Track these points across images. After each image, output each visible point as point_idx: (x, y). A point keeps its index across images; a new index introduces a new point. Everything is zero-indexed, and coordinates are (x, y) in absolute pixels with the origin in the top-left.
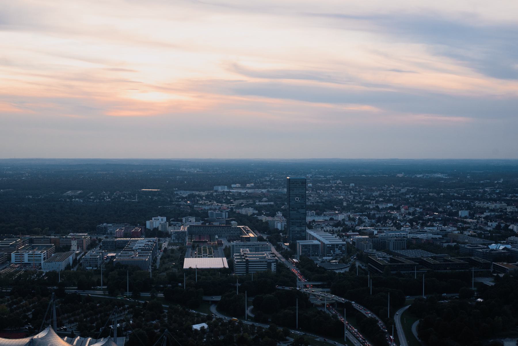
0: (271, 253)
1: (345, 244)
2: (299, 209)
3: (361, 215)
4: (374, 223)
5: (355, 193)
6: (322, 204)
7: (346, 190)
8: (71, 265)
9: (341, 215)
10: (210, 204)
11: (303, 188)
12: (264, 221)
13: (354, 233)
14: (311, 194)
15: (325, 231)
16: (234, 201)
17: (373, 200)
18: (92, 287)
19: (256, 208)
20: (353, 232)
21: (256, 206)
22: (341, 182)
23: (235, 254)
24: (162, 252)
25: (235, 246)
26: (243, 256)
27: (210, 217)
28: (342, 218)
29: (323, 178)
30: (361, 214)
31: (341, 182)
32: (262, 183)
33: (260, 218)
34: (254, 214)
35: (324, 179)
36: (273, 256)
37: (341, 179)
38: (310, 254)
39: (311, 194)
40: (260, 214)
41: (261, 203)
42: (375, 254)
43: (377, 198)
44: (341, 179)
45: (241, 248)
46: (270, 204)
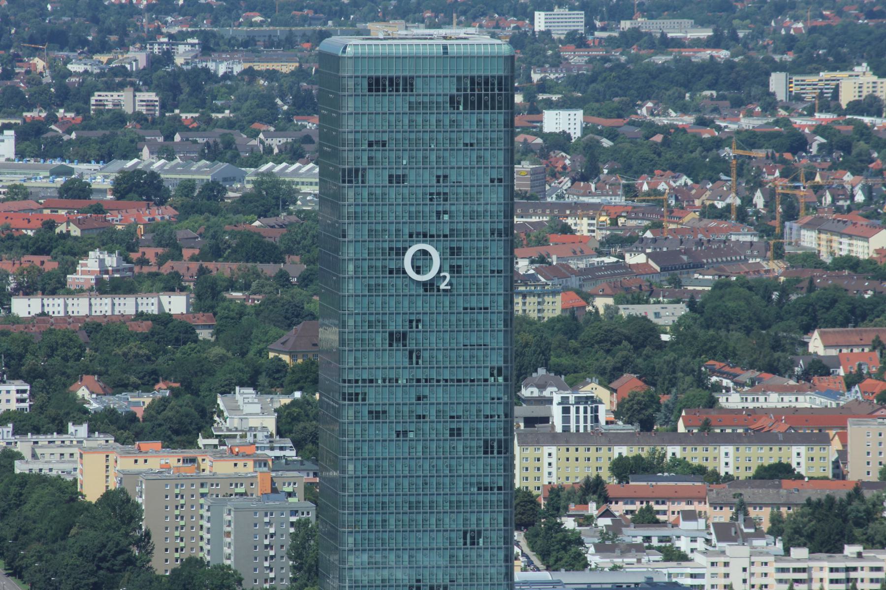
29: (698, 44)
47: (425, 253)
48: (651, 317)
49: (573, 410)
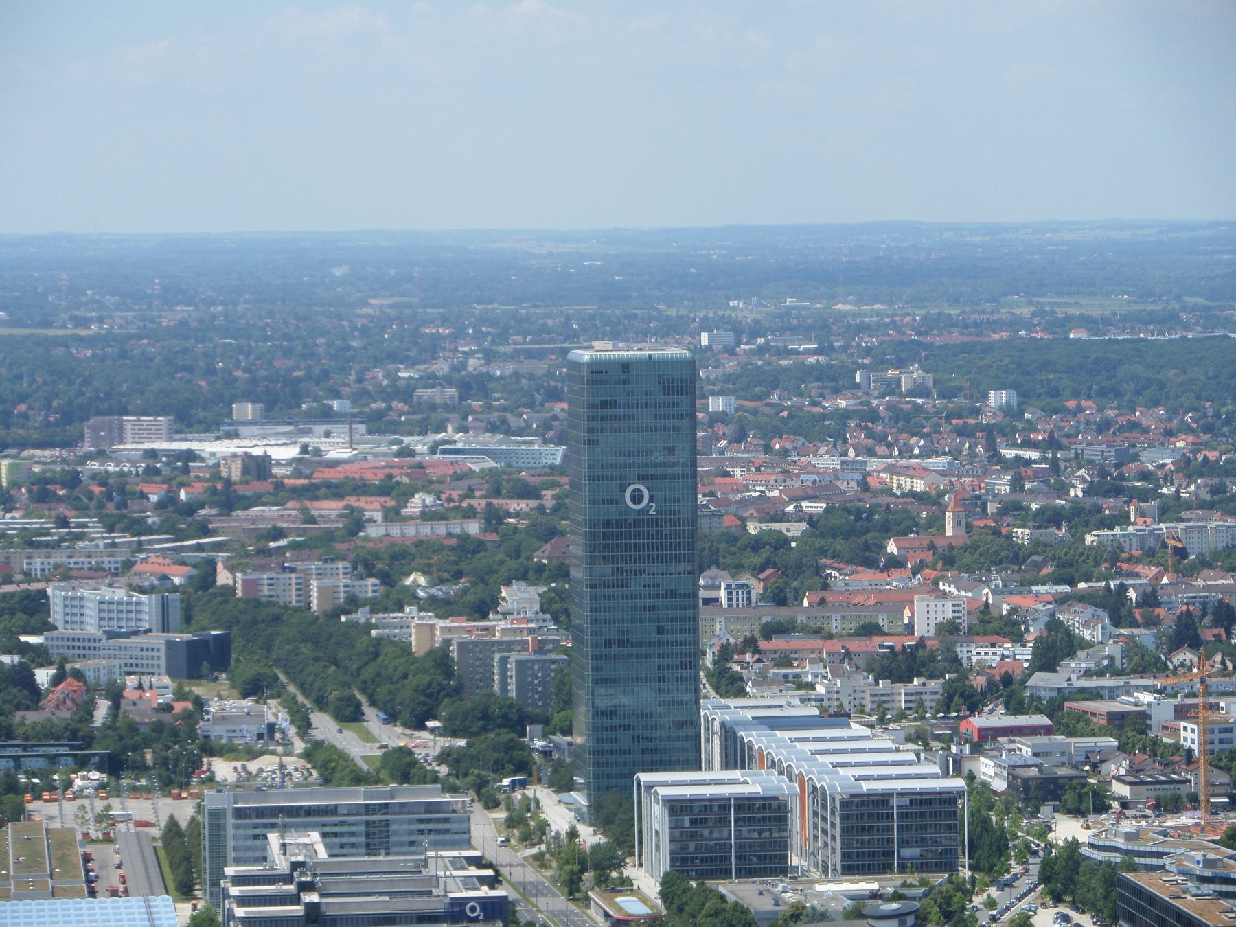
0: (478, 862)
1: (964, 792)
2: (1023, 874)
3: (1062, 600)
4: (1151, 647)
5: (1027, 454)
6: (804, 526)
7: (962, 432)
8: (368, 608)
9: (932, 604)
10: (62, 540)
11: (678, 422)
12: (418, 646)
13: (1022, 720)
14: (734, 461)
15: (830, 716)
16: (220, 515)
17: (1143, 496)
18: (36, 780)
19: (365, 565)
20: (1015, 708)
21: (371, 545)
22: (930, 378)
23: (230, 871)
24: (198, 690)
25: (229, 814)
26: (288, 879)
27: (60, 624)
28: (940, 619)
29: (808, 352)
30: (1066, 588)
31: (930, 378)
32: (405, 393)
33: (386, 625)
34: (353, 602)
35: (812, 360)
36: (483, 880)
37: (931, 357)
38: (725, 834)
39: (734, 461)
40: (398, 600)
41: (395, 530)
42: (1160, 855)
43: (1168, 480)
44: (931, 357)
45: (273, 826)
46: (458, 536)
47: (639, 490)
48: (784, 531)
49: (734, 593)
